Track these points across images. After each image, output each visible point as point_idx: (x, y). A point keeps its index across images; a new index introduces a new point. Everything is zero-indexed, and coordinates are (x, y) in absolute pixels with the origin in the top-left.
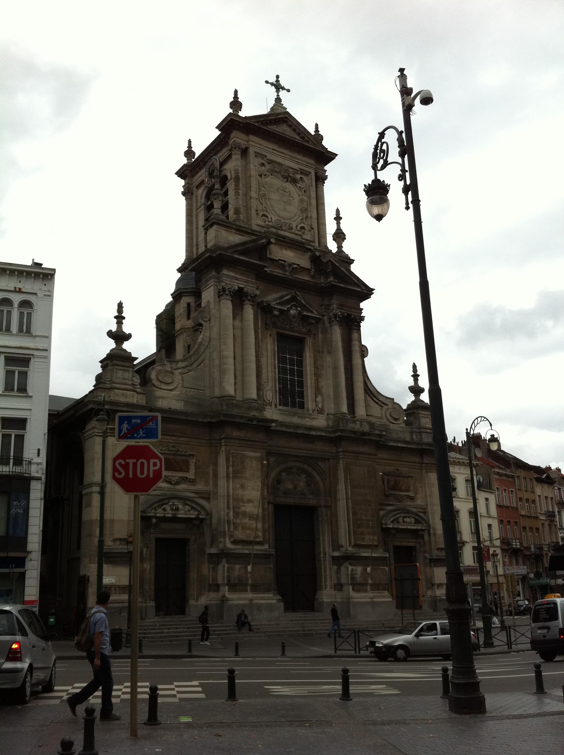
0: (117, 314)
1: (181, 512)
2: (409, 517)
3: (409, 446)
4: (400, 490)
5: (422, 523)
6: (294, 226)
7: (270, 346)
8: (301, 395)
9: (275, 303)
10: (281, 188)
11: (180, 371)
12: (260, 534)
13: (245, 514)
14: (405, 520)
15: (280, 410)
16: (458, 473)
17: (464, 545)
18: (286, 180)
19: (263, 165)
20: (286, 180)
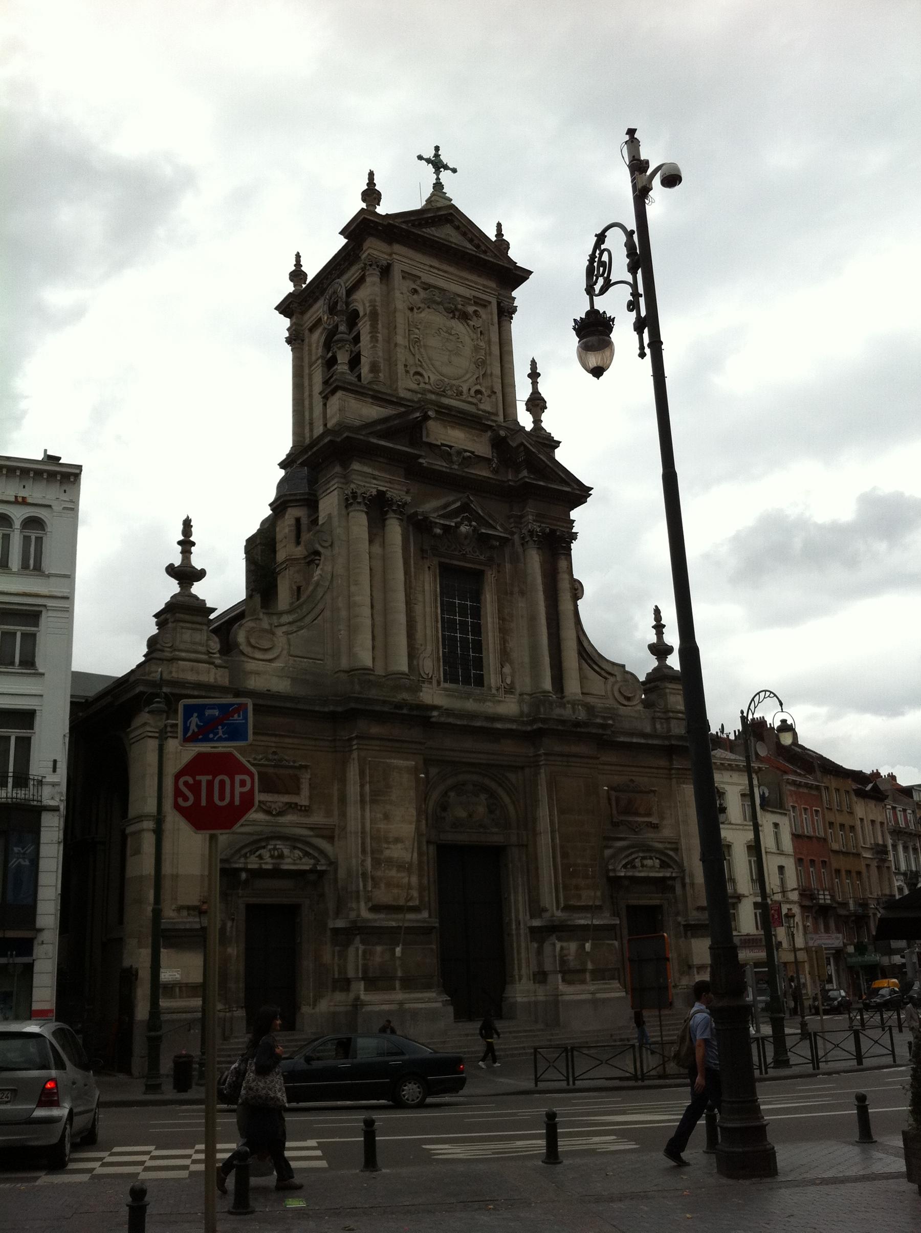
0: (182, 538)
2: (651, 858)
3: (650, 742)
4: (637, 814)
6: (465, 389)
7: (429, 585)
8: (479, 663)
9: (435, 515)
10: (445, 329)
11: (284, 629)
12: (415, 894)
13: (390, 862)
14: (646, 862)
15: (445, 689)
16: (728, 783)
17: (740, 901)
18: (451, 315)
19: (415, 291)
20: (451, 315)
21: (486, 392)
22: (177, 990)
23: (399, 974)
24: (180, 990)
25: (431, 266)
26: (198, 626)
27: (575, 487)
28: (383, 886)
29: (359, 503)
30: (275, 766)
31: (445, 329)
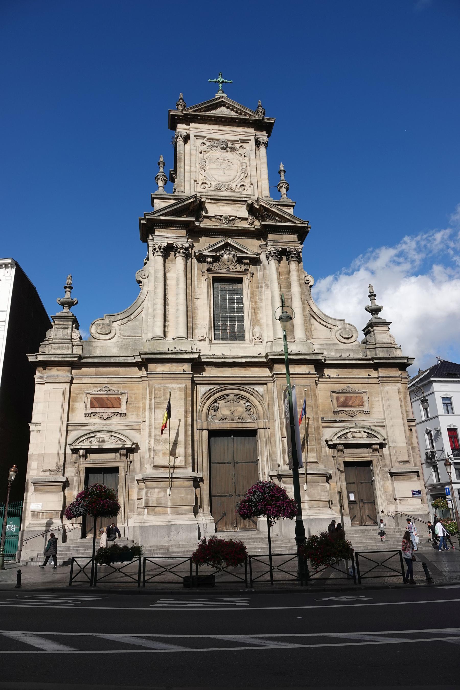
1: (106, 443)
4: (351, 406)
5: (376, 437)
7: (203, 289)
8: (242, 328)
9: (205, 252)
11: (119, 322)
14: (355, 435)
18: (225, 151)
21: (247, 185)
22: (41, 514)
23: (169, 504)
24: (43, 515)
25: (213, 129)
26: (66, 326)
28: (161, 454)
29: (157, 252)
30: (106, 394)
31: (221, 158)
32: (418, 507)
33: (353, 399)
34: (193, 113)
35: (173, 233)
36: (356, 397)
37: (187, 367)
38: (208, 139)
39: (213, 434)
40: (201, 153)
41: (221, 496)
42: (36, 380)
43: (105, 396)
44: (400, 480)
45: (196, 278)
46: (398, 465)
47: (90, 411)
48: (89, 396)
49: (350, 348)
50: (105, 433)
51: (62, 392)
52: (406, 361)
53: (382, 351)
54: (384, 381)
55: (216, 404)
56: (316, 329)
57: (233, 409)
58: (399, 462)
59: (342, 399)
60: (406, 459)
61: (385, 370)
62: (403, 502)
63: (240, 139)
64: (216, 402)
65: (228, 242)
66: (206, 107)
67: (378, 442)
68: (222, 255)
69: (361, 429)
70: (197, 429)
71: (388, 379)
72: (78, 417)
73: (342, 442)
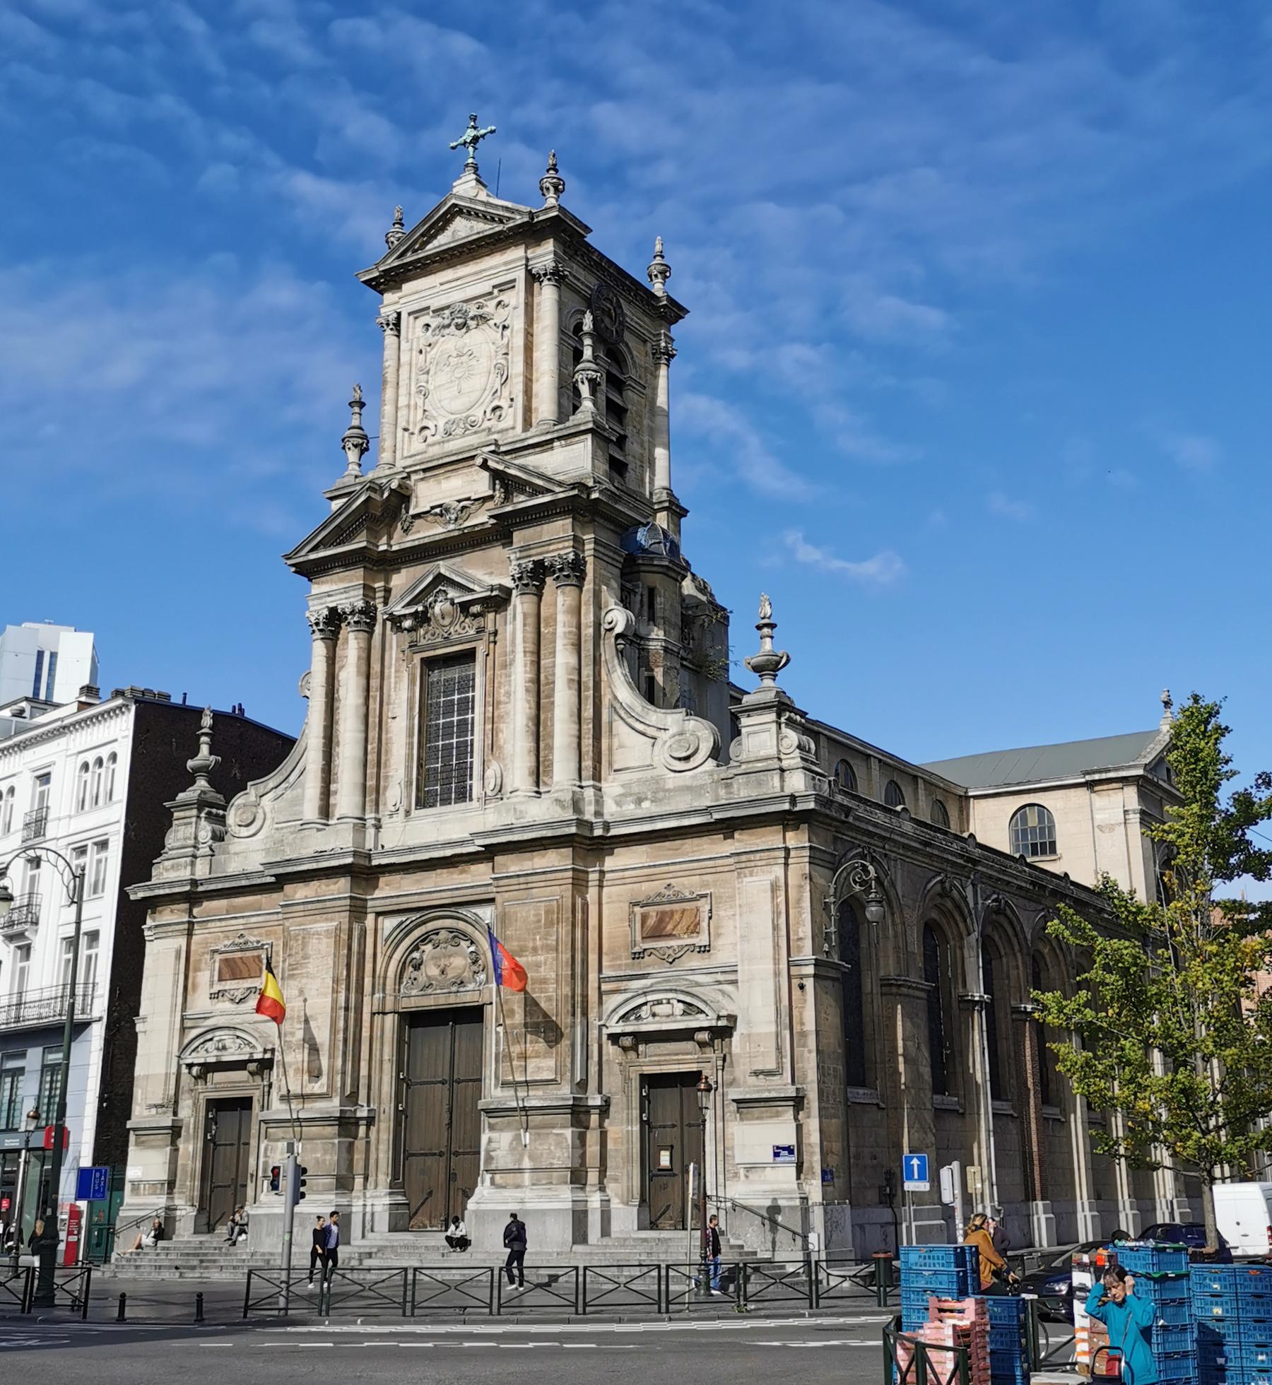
4: (670, 936)
5: (702, 1012)
9: (399, 608)
14: (657, 1009)
18: (464, 330)
27: (557, 489)
30: (241, 950)
32: (785, 1186)
33: (677, 917)
34: (396, 264)
35: (341, 580)
36: (683, 911)
37: (340, 888)
38: (434, 312)
39: (413, 1020)
40: (421, 352)
41: (425, 1155)
42: (146, 933)
43: (239, 954)
44: (752, 1119)
45: (393, 670)
46: (752, 1080)
47: (215, 989)
48: (218, 957)
49: (689, 783)
50: (227, 1032)
51: (173, 954)
52: (786, 806)
53: (747, 783)
54: (743, 865)
55: (416, 955)
56: (621, 746)
57: (443, 962)
58: (756, 1073)
59: (651, 922)
60: (772, 1065)
61: (751, 835)
62: (752, 1176)
63: (494, 287)
64: (417, 948)
65: (440, 574)
66: (422, 235)
67: (706, 1024)
68: (431, 606)
69: (670, 995)
70: (373, 1014)
71: (752, 857)
72: (200, 1002)
73: (629, 1029)
